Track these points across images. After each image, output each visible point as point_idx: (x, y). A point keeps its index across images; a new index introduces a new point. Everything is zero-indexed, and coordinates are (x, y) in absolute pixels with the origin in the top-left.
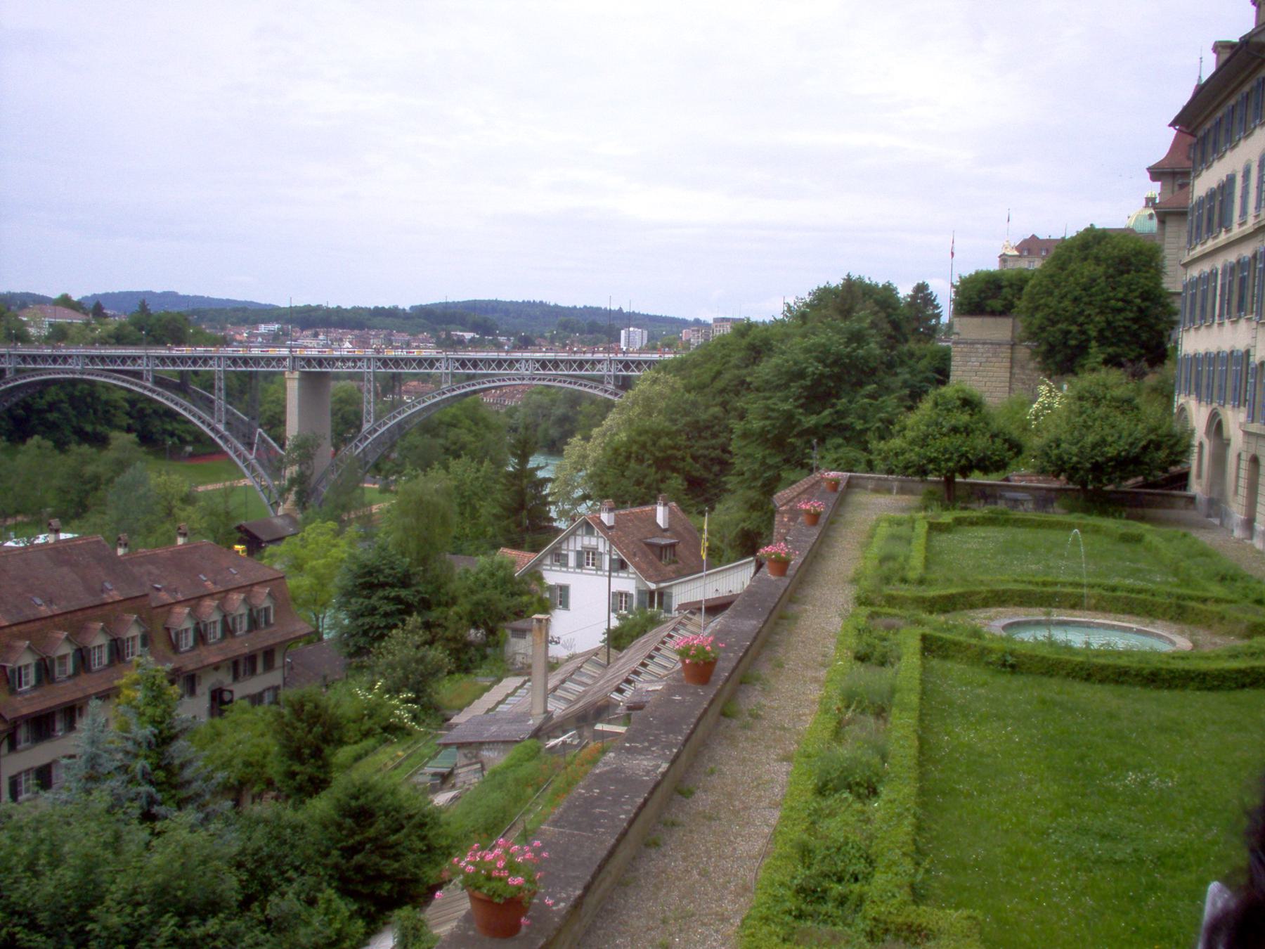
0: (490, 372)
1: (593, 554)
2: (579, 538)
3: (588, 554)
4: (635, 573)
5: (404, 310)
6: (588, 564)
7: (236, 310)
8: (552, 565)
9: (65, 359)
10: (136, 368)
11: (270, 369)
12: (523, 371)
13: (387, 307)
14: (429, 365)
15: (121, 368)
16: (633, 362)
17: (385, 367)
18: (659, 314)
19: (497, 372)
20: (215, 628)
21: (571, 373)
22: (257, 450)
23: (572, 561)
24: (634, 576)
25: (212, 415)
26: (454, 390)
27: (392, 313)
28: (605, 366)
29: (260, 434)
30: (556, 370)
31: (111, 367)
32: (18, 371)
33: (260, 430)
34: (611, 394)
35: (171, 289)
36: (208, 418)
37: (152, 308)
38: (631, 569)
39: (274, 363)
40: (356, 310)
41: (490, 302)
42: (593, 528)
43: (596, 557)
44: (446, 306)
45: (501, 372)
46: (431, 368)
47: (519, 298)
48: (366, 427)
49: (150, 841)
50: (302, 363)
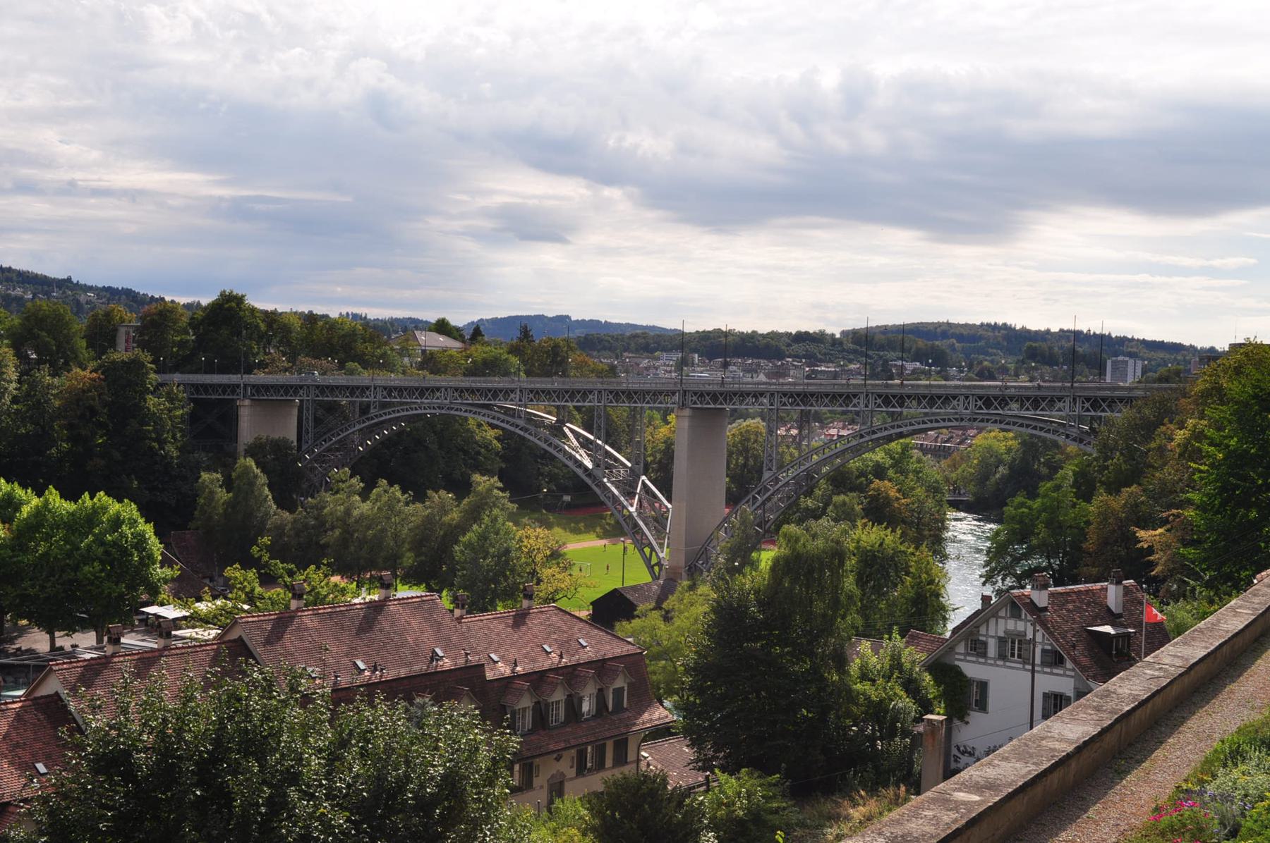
1: (1020, 642)
2: (1001, 622)
3: (1013, 642)
4: (1073, 670)
5: (833, 335)
6: (1013, 655)
7: (635, 336)
8: (967, 654)
11: (226, 397)
12: (961, 409)
13: (811, 332)
16: (1104, 400)
17: (197, 394)
18: (1158, 339)
20: (558, 709)
22: (640, 500)
23: (992, 650)
24: (1073, 674)
26: (381, 416)
29: (643, 481)
30: (887, 407)
32: (384, 405)
33: (644, 478)
35: (494, 316)
37: (539, 338)
38: (1069, 664)
40: (774, 335)
41: (939, 324)
42: (1020, 610)
43: (1024, 646)
44: (885, 330)
45: (934, 410)
47: (976, 320)
50: (694, 398)
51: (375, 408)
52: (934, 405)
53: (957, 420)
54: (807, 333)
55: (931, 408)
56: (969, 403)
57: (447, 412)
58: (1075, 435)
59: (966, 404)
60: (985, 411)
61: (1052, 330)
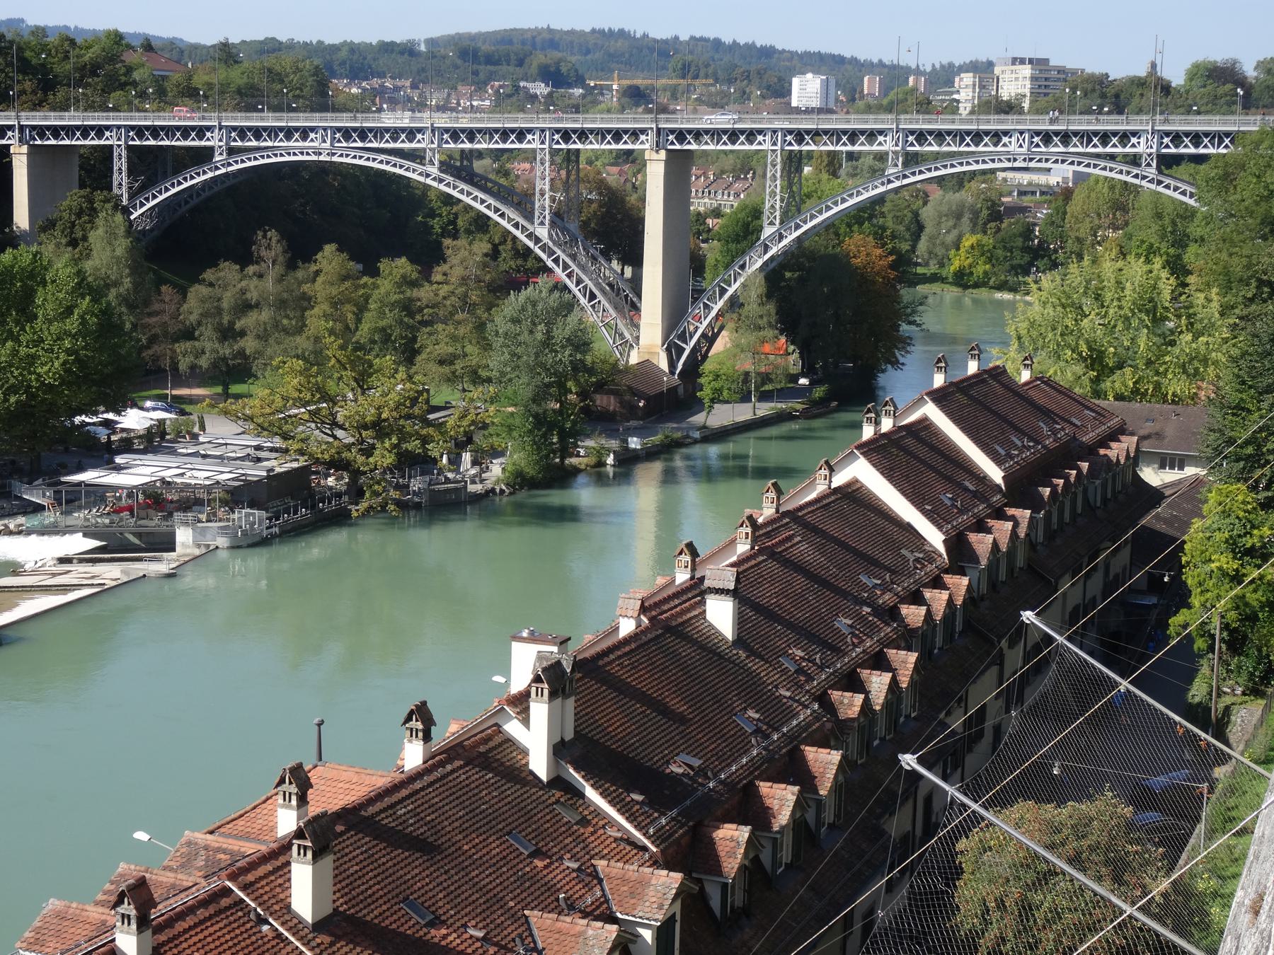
0: (276, 144)
9: (305, 133)
10: (414, 145)
12: (1013, 147)
14: (729, 139)
15: (391, 145)
17: (242, 140)
18: (813, 48)
19: (973, 148)
21: (1090, 150)
25: (529, 216)
27: (408, 50)
28: (1142, 140)
31: (375, 145)
34: (434, 179)
36: (522, 221)
39: (1115, 140)
41: (538, 31)
46: (996, 145)
48: (768, 231)
49: (303, 800)
51: (221, 154)
52: (507, 140)
53: (1009, 160)
54: (393, 44)
55: (977, 145)
56: (1024, 140)
57: (328, 159)
58: (1151, 176)
59: (1021, 141)
60: (345, 144)
61: (681, 39)
